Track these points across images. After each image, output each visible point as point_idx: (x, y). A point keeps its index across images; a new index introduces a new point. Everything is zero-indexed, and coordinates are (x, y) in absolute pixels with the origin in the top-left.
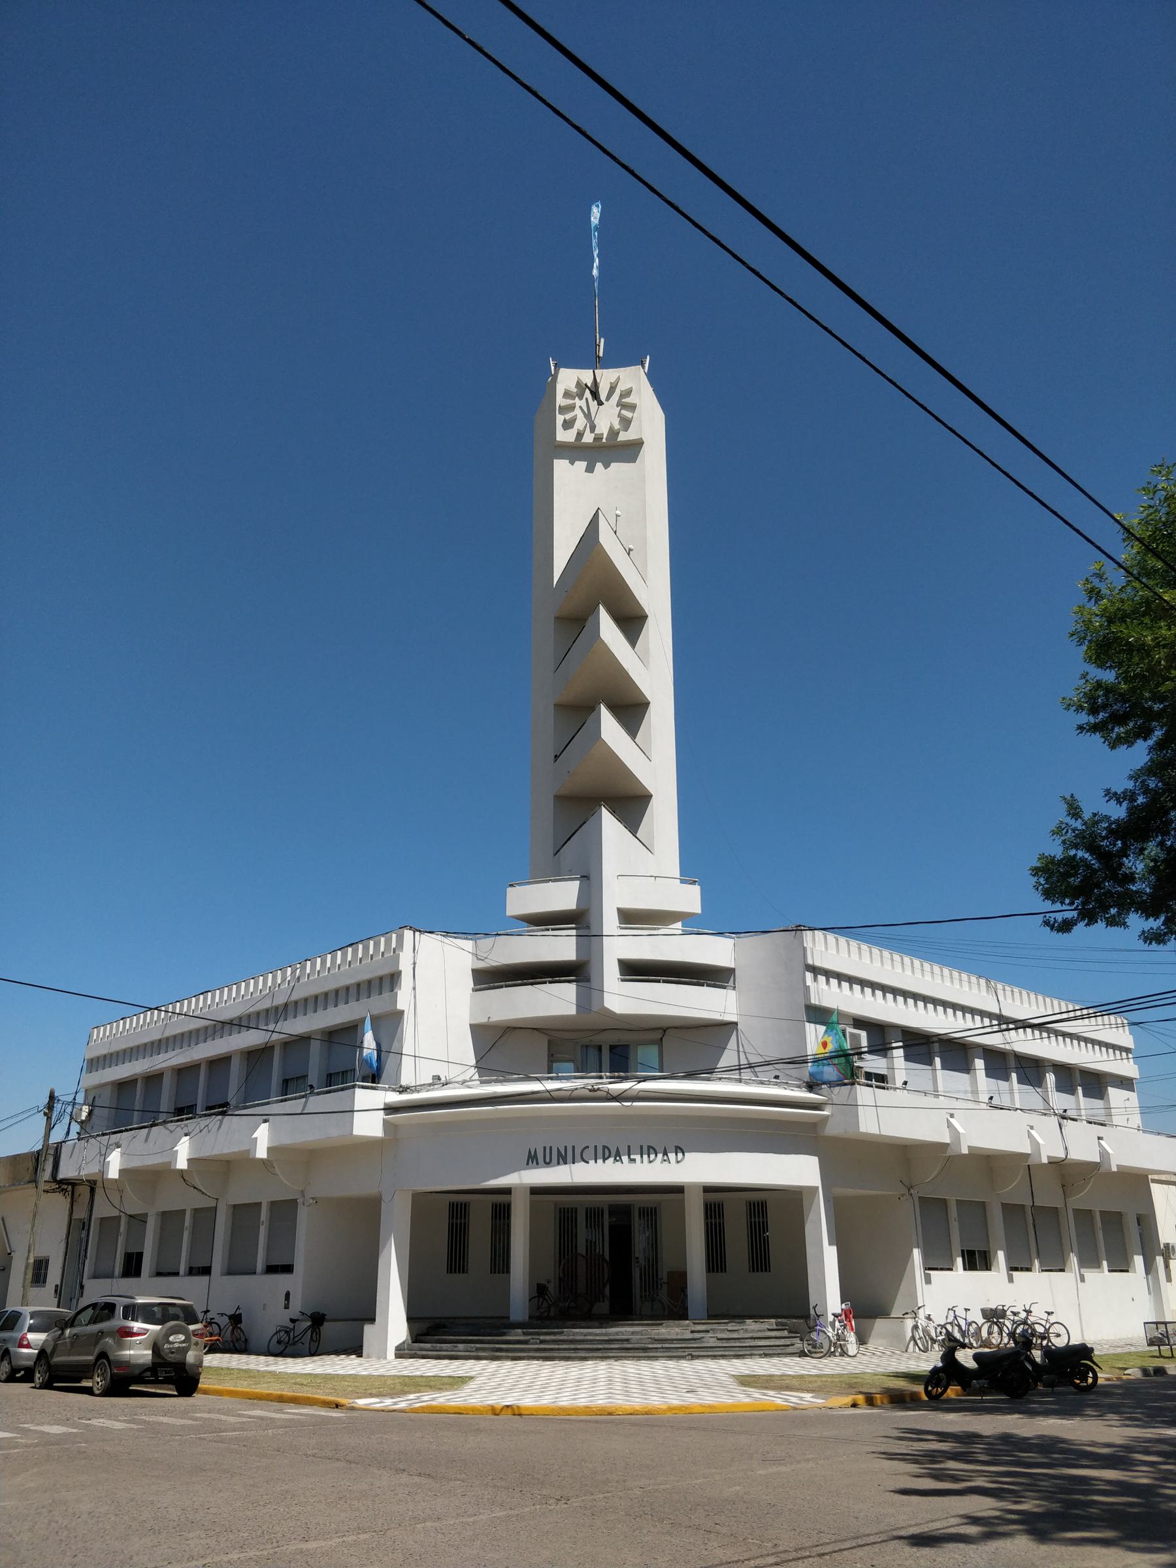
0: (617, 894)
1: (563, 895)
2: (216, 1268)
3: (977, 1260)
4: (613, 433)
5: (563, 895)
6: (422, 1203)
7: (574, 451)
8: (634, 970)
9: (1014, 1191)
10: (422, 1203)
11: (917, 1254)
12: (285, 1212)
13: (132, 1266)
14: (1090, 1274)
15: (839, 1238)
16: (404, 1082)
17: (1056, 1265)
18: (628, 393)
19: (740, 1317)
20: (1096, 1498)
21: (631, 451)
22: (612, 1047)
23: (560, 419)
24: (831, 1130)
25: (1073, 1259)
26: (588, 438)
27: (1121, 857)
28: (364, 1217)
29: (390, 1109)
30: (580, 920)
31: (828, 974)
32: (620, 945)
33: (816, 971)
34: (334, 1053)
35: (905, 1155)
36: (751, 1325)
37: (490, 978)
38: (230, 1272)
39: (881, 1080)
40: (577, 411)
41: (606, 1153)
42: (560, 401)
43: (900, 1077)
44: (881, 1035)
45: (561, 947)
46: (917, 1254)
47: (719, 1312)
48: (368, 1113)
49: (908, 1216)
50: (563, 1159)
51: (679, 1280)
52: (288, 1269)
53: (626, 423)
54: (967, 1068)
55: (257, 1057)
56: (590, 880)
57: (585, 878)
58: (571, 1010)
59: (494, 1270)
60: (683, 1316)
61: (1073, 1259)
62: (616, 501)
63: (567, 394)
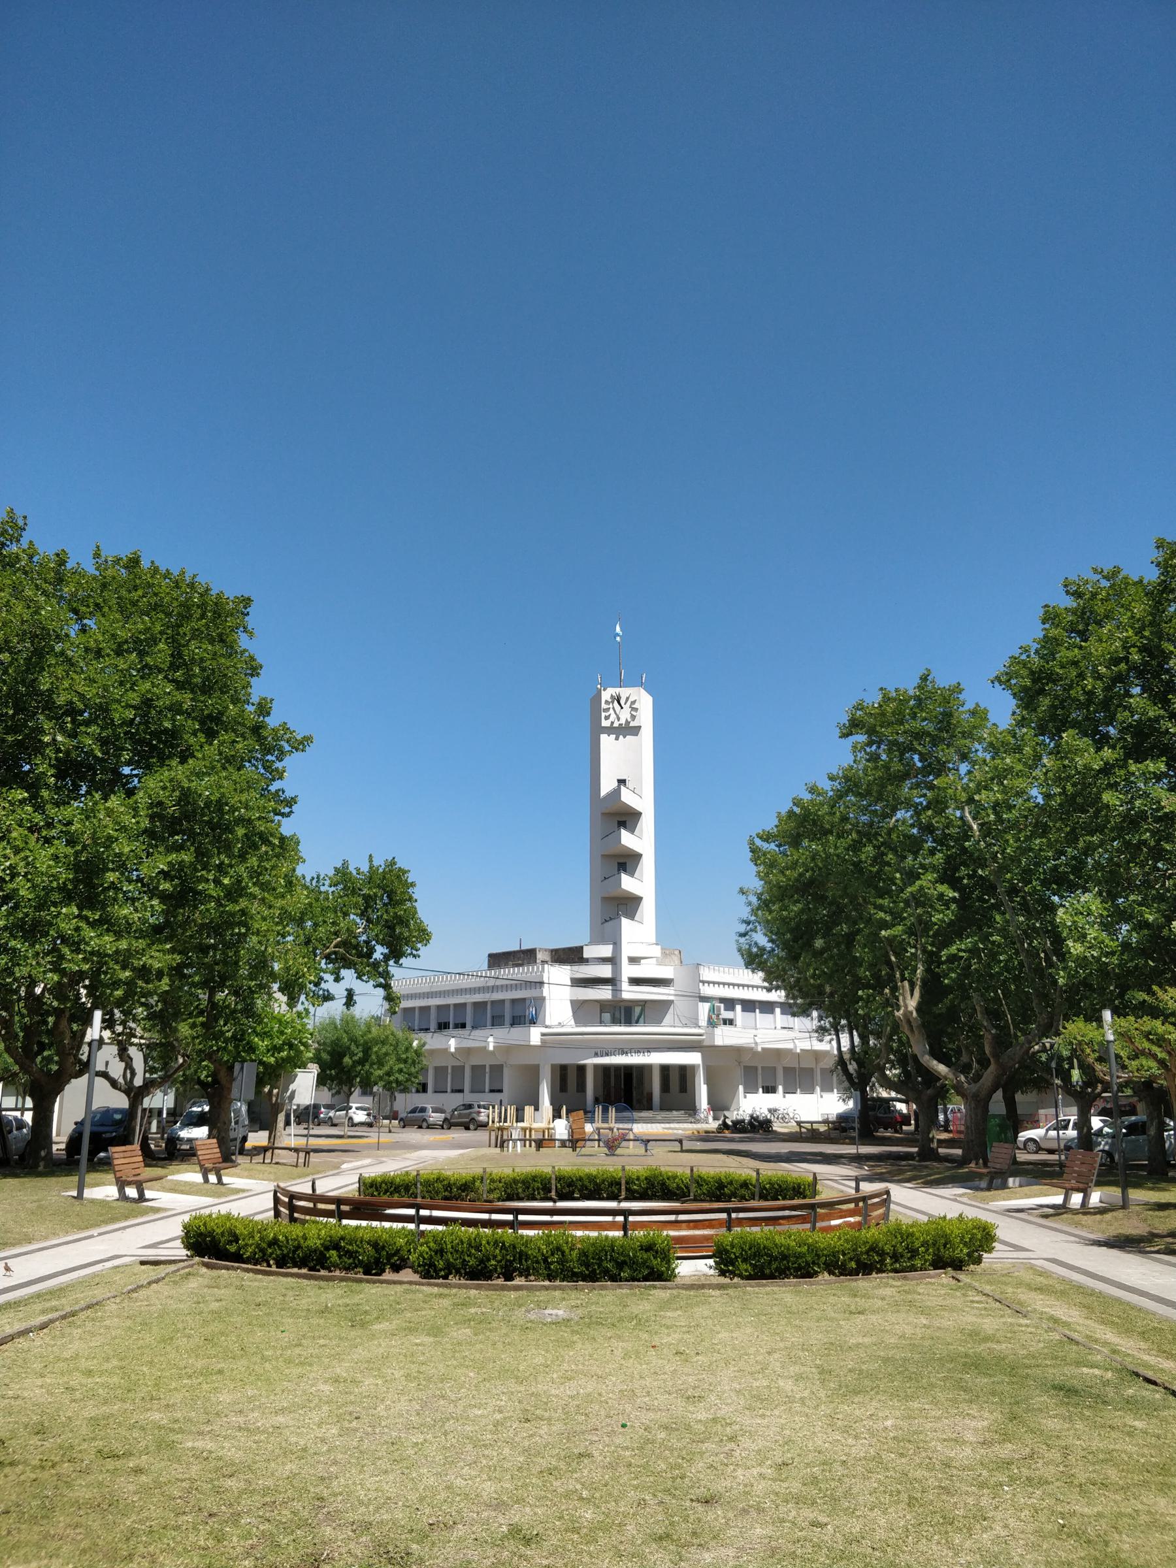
0: (627, 951)
1: (606, 951)
2: (467, 1088)
3: (770, 1090)
4: (627, 722)
5: (606, 951)
6: (553, 1066)
7: (610, 730)
8: (635, 981)
9: (787, 1062)
10: (553, 1066)
11: (741, 1088)
12: (497, 1070)
13: (423, 1088)
14: (825, 1095)
15: (708, 1082)
16: (547, 1023)
17: (810, 1090)
18: (634, 702)
19: (670, 1110)
20: (613, 1084)
21: (636, 731)
22: (624, 1012)
23: (603, 714)
24: (706, 1044)
25: (818, 1089)
26: (616, 724)
27: (1080, 723)
28: (532, 1073)
29: (543, 1035)
30: (613, 961)
31: (709, 983)
32: (628, 971)
33: (704, 982)
34: (523, 1013)
35: (737, 1051)
36: (675, 1113)
37: (579, 982)
38: (472, 1091)
39: (730, 1022)
40: (611, 711)
41: (623, 1052)
42: (604, 706)
43: (739, 1021)
44: (730, 1003)
45: (605, 971)
46: (741, 1088)
47: (663, 1108)
48: (535, 1035)
49: (739, 1073)
50: (607, 1055)
51: (650, 1096)
52: (500, 1091)
53: (633, 717)
54: (772, 1012)
55: (479, 1006)
56: (617, 944)
57: (615, 944)
58: (610, 997)
59: (578, 1091)
60: (651, 1109)
61: (818, 1089)
62: (629, 764)
63: (607, 702)
